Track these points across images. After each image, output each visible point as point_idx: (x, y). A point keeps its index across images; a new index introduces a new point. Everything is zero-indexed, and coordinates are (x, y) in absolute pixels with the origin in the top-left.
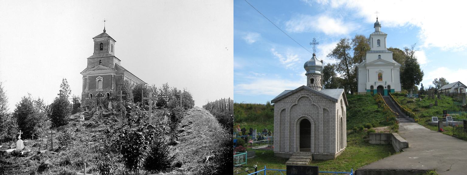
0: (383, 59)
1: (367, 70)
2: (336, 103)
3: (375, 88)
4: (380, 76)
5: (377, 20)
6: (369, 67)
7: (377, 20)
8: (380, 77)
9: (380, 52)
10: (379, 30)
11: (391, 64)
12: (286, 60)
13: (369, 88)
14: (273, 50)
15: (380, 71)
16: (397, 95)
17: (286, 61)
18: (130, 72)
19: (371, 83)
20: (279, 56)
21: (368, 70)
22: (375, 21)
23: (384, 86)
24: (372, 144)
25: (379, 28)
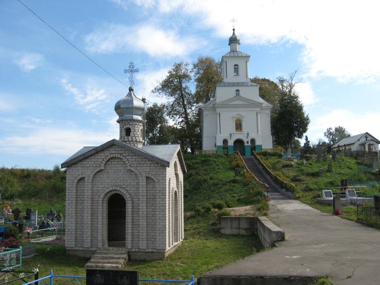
0: (243, 96)
2: (167, 168)
3: (231, 143)
5: (234, 32)
6: (221, 109)
7: (234, 32)
8: (239, 126)
9: (238, 84)
11: (256, 104)
12: (86, 98)
13: (220, 143)
14: (64, 81)
16: (265, 154)
20: (75, 91)
22: (231, 34)
23: (245, 140)
25: (236, 46)
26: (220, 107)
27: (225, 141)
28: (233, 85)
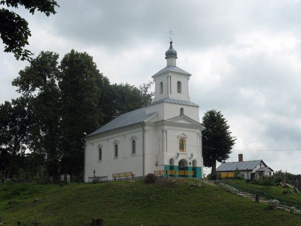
0: (186, 115)
2: (282, 171)
3: (176, 163)
5: (171, 47)
6: (168, 127)
7: (171, 47)
8: (182, 147)
11: (198, 125)
13: (167, 163)
15: (183, 136)
18: (167, 137)
23: (189, 161)
26: (168, 125)
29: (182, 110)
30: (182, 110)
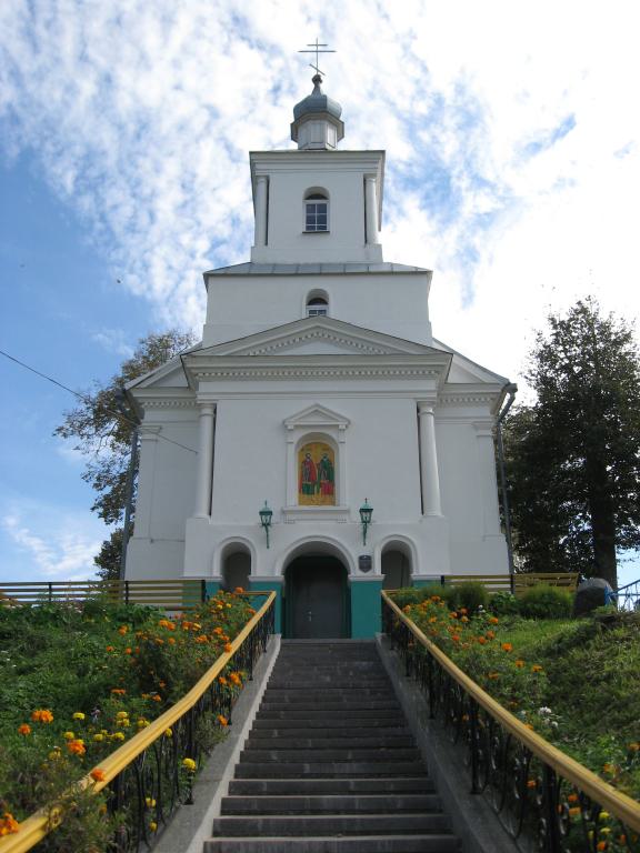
1: (199, 407)
3: (268, 566)
4: (316, 457)
8: (318, 477)
9: (321, 272)
10: (323, 142)
12: (60, 561)
13: (205, 565)
14: (11, 521)
16: (466, 599)
17: (60, 566)
19: (232, 521)
20: (36, 544)
21: (209, 411)
22: (306, 90)
23: (352, 552)
24: (474, 784)
25: (323, 135)
27: (237, 560)
28: (297, 273)
29: (317, 300)
30: (317, 300)
